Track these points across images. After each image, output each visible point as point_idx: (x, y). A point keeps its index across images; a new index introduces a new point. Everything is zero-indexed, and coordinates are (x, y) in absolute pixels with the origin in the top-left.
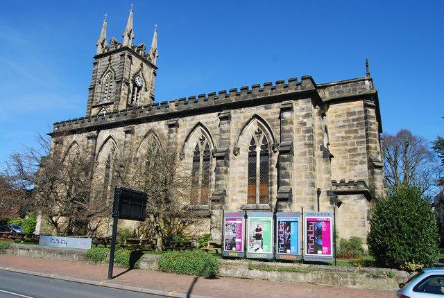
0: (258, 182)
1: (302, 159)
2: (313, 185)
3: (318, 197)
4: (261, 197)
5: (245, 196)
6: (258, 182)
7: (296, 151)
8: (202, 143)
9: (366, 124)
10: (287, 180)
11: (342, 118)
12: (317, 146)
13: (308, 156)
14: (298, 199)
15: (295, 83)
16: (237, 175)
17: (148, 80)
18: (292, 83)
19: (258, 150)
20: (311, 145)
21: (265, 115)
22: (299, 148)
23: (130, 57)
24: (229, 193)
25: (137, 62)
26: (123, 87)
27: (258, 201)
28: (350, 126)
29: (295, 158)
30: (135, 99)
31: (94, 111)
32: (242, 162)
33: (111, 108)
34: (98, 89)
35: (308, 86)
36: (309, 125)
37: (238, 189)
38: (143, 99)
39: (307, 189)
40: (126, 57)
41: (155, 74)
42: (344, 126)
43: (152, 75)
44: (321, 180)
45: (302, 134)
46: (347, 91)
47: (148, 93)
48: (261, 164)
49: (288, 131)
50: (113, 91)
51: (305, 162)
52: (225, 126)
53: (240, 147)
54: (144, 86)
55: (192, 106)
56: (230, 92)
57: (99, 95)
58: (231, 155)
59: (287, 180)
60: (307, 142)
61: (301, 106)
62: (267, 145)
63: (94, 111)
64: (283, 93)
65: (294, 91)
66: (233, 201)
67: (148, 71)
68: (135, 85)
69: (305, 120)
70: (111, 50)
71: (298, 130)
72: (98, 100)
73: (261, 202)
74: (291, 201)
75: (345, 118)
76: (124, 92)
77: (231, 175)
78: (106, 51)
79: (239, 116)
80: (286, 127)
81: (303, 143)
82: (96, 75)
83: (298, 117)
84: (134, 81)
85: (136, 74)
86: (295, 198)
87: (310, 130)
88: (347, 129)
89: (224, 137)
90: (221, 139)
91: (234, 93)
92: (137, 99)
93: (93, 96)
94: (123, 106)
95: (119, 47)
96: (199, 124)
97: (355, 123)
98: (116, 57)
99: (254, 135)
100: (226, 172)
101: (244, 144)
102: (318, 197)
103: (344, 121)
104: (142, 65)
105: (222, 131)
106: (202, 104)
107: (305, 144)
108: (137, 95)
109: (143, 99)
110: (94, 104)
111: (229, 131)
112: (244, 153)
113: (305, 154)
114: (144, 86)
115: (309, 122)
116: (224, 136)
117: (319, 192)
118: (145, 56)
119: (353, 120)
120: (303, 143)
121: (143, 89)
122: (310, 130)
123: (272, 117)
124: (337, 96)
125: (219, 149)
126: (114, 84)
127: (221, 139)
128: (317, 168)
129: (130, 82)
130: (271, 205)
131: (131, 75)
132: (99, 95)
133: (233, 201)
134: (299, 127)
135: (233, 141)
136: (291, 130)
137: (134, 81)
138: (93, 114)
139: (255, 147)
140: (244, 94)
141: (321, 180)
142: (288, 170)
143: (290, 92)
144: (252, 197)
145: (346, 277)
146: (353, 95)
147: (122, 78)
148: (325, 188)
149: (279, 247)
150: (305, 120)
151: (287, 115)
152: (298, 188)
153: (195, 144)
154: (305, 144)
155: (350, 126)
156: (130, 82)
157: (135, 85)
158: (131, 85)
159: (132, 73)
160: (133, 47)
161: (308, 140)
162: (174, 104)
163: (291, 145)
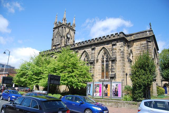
0: (105, 71)
1: (120, 62)
2: (124, 72)
3: (126, 76)
4: (106, 76)
5: (101, 76)
6: (105, 71)
7: (118, 60)
8: (105, 55)
9: (147, 48)
10: (114, 70)
11: (138, 46)
12: (126, 57)
13: (122, 61)
14: (119, 77)
15: (117, 35)
16: (98, 69)
17: (72, 35)
18: (108, 37)
19: (105, 59)
20: (123, 57)
21: (107, 47)
22: (118, 58)
23: (65, 28)
24: (95, 75)
25: (67, 30)
26: (63, 38)
27: (105, 78)
28: (142, 49)
29: (117, 62)
30: (67, 42)
31: (54, 48)
32: (99, 64)
33: (59, 46)
34: (55, 40)
35: (122, 35)
36: (122, 50)
37: (98, 74)
38: (70, 42)
39: (121, 73)
40: (64, 28)
41: (74, 33)
42: (139, 49)
43: (73, 34)
44: (127, 70)
45: (119, 53)
46: (140, 36)
47: (72, 40)
48: (106, 65)
49: (114, 53)
50: (60, 40)
51: (121, 64)
52: (93, 52)
53: (99, 59)
54: (71, 37)
55: (83, 45)
56: (95, 39)
57: (55, 41)
58: (96, 62)
59: (114, 70)
60: (121, 56)
61: (119, 44)
62: (108, 58)
63: (54, 48)
64: (113, 39)
65: (117, 38)
66: (96, 78)
67: (72, 32)
68: (67, 37)
69: (121, 48)
70: (59, 25)
71: (118, 52)
72: (55, 43)
73: (106, 78)
74: (115, 78)
75: (140, 46)
76: (63, 40)
77: (95, 69)
78: (57, 26)
79: (98, 48)
80: (114, 51)
81: (120, 56)
82: (54, 35)
83: (118, 47)
84: (67, 36)
85: (68, 34)
86: (117, 77)
87: (123, 52)
88: (140, 50)
89: (93, 55)
90: (92, 56)
91: (96, 40)
92: (68, 42)
93: (53, 42)
94: (63, 45)
95: (61, 24)
96: (103, 48)
97: (143, 48)
98: (60, 28)
99: (103, 54)
100: (93, 68)
101: (100, 57)
102: (126, 76)
103: (139, 47)
104: (69, 30)
105: (92, 53)
106: (86, 44)
107: (121, 57)
108: (68, 41)
109: (70, 42)
110: (53, 45)
111: (95, 53)
112: (100, 61)
113: (120, 60)
114: (71, 37)
115: (122, 49)
116: (93, 55)
117: (127, 75)
118: (71, 27)
119: (143, 47)
120: (120, 56)
121: (70, 39)
122: (123, 52)
123: (109, 48)
124: (137, 38)
125: (112, 57)
126: (60, 37)
127: (92, 56)
128: (126, 65)
129: (65, 36)
130: (109, 79)
131: (66, 34)
132: (55, 41)
133: (96, 78)
134: (119, 51)
135: (96, 57)
136: (116, 52)
137: (67, 36)
138: (53, 48)
139: (104, 59)
140: (112, 37)
141: (127, 70)
142: (114, 67)
143: (115, 38)
144: (103, 77)
145: (122, 104)
146: (142, 37)
147: (62, 35)
148: (129, 73)
149: (113, 94)
150: (121, 48)
151: (114, 47)
152: (119, 73)
153: (84, 58)
154: (121, 57)
155: (142, 49)
156: (65, 36)
157: (67, 37)
158: (66, 38)
159: (66, 33)
160: (66, 24)
161: (122, 55)
162: (77, 44)
163: (116, 58)
